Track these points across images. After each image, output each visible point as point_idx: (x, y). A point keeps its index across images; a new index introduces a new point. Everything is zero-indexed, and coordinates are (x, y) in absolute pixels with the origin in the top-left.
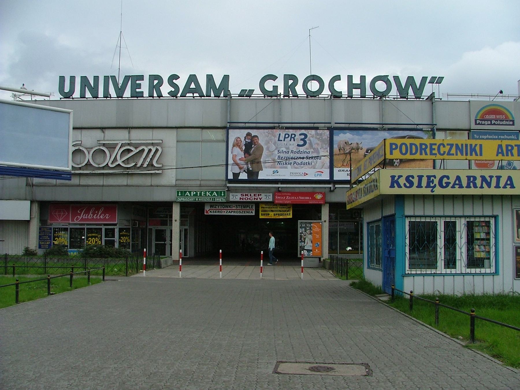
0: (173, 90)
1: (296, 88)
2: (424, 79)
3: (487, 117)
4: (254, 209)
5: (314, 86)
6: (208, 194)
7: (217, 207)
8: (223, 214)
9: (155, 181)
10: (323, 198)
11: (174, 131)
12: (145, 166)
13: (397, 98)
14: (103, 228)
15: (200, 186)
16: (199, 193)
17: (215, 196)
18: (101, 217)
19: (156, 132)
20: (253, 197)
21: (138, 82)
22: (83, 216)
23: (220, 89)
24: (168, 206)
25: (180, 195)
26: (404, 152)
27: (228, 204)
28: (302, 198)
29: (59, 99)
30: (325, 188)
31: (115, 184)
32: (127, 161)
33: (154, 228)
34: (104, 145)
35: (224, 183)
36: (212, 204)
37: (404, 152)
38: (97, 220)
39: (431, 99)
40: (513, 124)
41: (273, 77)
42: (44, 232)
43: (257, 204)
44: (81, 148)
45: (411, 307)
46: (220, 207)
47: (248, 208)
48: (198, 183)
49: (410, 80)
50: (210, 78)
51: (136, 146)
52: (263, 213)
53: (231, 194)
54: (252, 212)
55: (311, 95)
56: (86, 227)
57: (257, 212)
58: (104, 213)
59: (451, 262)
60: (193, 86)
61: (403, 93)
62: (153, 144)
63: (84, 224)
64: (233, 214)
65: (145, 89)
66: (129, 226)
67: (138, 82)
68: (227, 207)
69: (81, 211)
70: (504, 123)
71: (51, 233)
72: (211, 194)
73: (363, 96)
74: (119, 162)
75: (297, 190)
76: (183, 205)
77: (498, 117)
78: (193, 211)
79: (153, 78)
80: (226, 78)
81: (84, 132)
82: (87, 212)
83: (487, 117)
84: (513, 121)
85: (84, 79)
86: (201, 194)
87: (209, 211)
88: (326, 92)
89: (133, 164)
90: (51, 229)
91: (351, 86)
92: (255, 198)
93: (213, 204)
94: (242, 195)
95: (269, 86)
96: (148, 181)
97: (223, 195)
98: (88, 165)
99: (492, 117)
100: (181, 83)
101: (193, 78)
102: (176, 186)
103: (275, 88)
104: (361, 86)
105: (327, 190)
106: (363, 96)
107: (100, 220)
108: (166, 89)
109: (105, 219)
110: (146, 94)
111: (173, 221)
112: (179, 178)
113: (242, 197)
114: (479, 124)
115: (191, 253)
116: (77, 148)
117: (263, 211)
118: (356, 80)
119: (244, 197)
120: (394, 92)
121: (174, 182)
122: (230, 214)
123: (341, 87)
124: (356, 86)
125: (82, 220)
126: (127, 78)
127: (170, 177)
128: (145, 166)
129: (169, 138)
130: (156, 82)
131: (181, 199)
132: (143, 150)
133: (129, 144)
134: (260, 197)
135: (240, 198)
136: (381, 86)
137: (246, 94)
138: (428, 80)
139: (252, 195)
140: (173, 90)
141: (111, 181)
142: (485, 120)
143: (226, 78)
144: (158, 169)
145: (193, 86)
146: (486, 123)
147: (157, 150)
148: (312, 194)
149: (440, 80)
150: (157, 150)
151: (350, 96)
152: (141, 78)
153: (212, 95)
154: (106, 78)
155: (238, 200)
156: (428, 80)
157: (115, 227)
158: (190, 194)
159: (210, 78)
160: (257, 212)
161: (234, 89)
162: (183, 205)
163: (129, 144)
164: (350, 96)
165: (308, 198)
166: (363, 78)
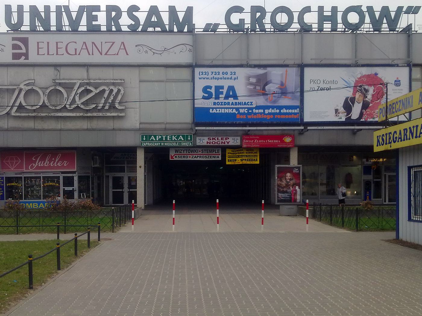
0: (133, 23)
1: (263, 20)
2: (400, 9)
4: (220, 153)
5: (282, 19)
6: (174, 138)
7: (182, 152)
8: (189, 159)
9: (118, 124)
10: (293, 141)
11: (136, 71)
12: (107, 108)
13: (369, 31)
14: (61, 176)
15: (165, 129)
16: (164, 137)
17: (181, 140)
18: (59, 164)
19: (116, 70)
20: (221, 141)
21: (94, 13)
22: (38, 163)
23: (182, 23)
24: (129, 153)
25: (144, 139)
26: (189, 152)
27: (195, 148)
28: (271, 141)
29: (6, 32)
30: (294, 130)
31: (73, 128)
32: (85, 103)
33: (111, 175)
34: (60, 84)
35: (189, 126)
36: (177, 149)
37: (189, 152)
38: (54, 167)
39: (409, 30)
41: (238, 9)
43: (224, 149)
44: (34, 88)
46: (185, 151)
47: (214, 153)
48: (163, 126)
49: (385, 10)
50: (172, 10)
51: (96, 86)
52: (229, 159)
53: (198, 138)
55: (281, 29)
56: (42, 175)
57: (224, 156)
58: (62, 159)
60: (154, 19)
61: (376, 24)
62: (114, 84)
63: (40, 173)
64: (198, 159)
65: (102, 19)
66: (89, 173)
67: (94, 13)
68: (192, 151)
69: (36, 158)
71: (3, 183)
72: (177, 138)
73: (334, 29)
74: (79, 102)
75: (265, 133)
76: (147, 150)
78: (158, 157)
79: (110, 9)
80: (189, 11)
81: (37, 69)
82: (43, 159)
85: (34, 10)
86: (166, 138)
87: (174, 156)
88: (295, 26)
89: (94, 106)
90: (2, 178)
91: (322, 18)
92: (222, 142)
93: (178, 149)
94: (209, 139)
95: (235, 19)
96: (110, 124)
97: (189, 139)
98: (44, 106)
100: (142, 17)
101: (154, 10)
102: (140, 130)
103: (242, 21)
104: (333, 19)
105: (296, 132)
106: (334, 29)
107: (58, 167)
108: (125, 21)
109: (63, 167)
110: (104, 28)
111: (138, 168)
112: (142, 121)
113: (209, 141)
115: (151, 202)
116: (30, 88)
117: (229, 157)
119: (211, 141)
120: (367, 26)
121: (137, 126)
123: (311, 19)
124: (327, 19)
125: (38, 167)
126: (82, 9)
127: (133, 119)
128: (107, 108)
129: (131, 77)
130: (114, 14)
131: (145, 145)
132: (104, 91)
133: (88, 84)
134: (228, 141)
135: (207, 142)
136: (353, 18)
137: (211, 28)
138: (404, 10)
139: (220, 138)
140: (133, 23)
141: (70, 125)
143: (189, 11)
144: (122, 111)
145: (154, 19)
147: (119, 91)
148: (280, 137)
149: (413, 10)
150: (119, 91)
151: (321, 29)
152: (97, 8)
153: (175, 30)
154: (58, 8)
155: (205, 144)
156: (404, 10)
157: (74, 175)
158: (156, 138)
159: (172, 10)
160: (224, 156)
161: (199, 22)
162: (147, 150)
163: (88, 84)
164: (321, 29)
165: (277, 141)
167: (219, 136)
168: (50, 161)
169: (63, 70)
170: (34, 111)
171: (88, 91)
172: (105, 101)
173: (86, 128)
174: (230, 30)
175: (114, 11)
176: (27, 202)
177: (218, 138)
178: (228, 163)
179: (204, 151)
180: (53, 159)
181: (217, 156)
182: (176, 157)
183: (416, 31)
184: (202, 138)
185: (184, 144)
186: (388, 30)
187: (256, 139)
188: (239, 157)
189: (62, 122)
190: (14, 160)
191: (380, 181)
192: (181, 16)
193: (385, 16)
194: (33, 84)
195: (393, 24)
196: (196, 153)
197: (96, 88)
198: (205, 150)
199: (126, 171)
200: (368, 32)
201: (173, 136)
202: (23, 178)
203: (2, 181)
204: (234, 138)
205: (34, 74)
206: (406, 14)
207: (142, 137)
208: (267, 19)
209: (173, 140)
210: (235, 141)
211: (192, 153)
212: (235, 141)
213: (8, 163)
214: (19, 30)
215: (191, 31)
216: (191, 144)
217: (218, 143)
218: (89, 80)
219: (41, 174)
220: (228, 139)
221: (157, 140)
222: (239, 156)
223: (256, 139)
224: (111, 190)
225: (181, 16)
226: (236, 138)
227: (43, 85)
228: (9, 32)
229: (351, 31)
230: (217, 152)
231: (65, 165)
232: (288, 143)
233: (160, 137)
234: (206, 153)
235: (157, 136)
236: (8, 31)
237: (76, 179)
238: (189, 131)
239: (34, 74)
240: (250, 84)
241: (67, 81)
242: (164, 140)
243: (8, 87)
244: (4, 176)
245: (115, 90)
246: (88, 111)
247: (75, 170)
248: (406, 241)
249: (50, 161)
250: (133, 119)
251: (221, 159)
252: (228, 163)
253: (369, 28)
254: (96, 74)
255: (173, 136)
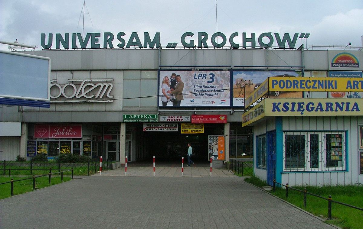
2: (296, 35)
3: (340, 61)
5: (219, 40)
7: (151, 126)
9: (108, 108)
10: (225, 119)
13: (277, 49)
14: (72, 141)
16: (139, 116)
17: (150, 118)
18: (71, 134)
19: (108, 72)
21: (96, 38)
22: (58, 133)
23: (154, 43)
24: (117, 125)
25: (125, 117)
27: (160, 123)
28: (211, 119)
29: (41, 50)
31: (80, 110)
33: (108, 141)
34: (73, 82)
35: (156, 109)
36: (148, 124)
38: (68, 136)
40: (358, 67)
41: (191, 34)
42: (31, 144)
43: (180, 124)
45: (287, 195)
46: (153, 125)
48: (138, 109)
49: (287, 36)
50: (146, 35)
53: (161, 117)
54: (176, 129)
55: (217, 46)
56: (60, 141)
58: (73, 130)
59: (315, 163)
60: (135, 40)
61: (281, 45)
62: (106, 82)
63: (58, 139)
64: (162, 131)
65: (101, 42)
67: (96, 38)
69: (57, 130)
70: (352, 65)
71: (35, 145)
72: (147, 117)
73: (253, 47)
75: (207, 114)
76: (128, 125)
77: (348, 61)
78: (135, 129)
79: (107, 34)
80: (158, 35)
81: (59, 73)
82: (61, 130)
83: (340, 61)
84: (358, 64)
85: (59, 36)
86: (140, 117)
87: (146, 129)
89: (93, 96)
90: (35, 142)
91: (245, 40)
93: (149, 124)
95: (188, 40)
97: (155, 117)
98: (62, 96)
99: (344, 61)
101: (134, 35)
102: (123, 111)
103: (192, 41)
104: (252, 40)
105: (228, 113)
106: (253, 47)
107: (70, 135)
108: (116, 43)
109: (73, 135)
111: (121, 136)
112: (124, 106)
114: (334, 66)
116: (54, 85)
118: (249, 36)
119: (171, 119)
120: (275, 44)
121: (121, 109)
122: (160, 131)
123: (238, 41)
126: (89, 35)
129: (118, 77)
131: (126, 121)
132: (100, 86)
133: (90, 82)
134: (182, 118)
135: (168, 120)
136: (266, 40)
137: (172, 46)
139: (176, 117)
140: (121, 43)
142: (338, 64)
143: (158, 35)
144: (110, 99)
145: (135, 40)
146: (339, 65)
147: (110, 86)
148: (217, 116)
149: (307, 36)
150: (110, 86)
151: (244, 47)
152: (98, 34)
153: (148, 47)
154: (74, 35)
155: (166, 121)
157: (80, 141)
158: (133, 117)
159: (146, 35)
161: (164, 43)
162: (128, 125)
163: (90, 82)
164: (244, 47)
165: (215, 119)
166: (253, 35)
167: (176, 116)
168: (65, 131)
169: (75, 73)
170: (56, 99)
171: (90, 86)
172: (303, 171)
173: (88, 110)
174: (185, 47)
175: (109, 37)
176: (50, 158)
177: (175, 117)
178: (182, 133)
179: (166, 125)
180: (67, 130)
181: (175, 128)
182: (147, 129)
183: (308, 49)
184: (164, 117)
185: (152, 121)
186: (289, 48)
187: (201, 117)
188: (190, 128)
189: (73, 106)
190: (43, 131)
191: (125, 166)
192: (152, 38)
193: (287, 39)
194: (56, 82)
195: (292, 44)
196: (160, 127)
197: (95, 84)
198: (167, 125)
199: (117, 139)
200: (276, 49)
201: (145, 116)
202: (60, 142)
203: (35, 144)
204: (186, 117)
205: (57, 76)
206: (301, 38)
207: (124, 116)
208: (209, 43)
209: (145, 118)
210: (187, 119)
211: (158, 127)
212: (187, 119)
213: (39, 132)
214: (50, 48)
215: (159, 46)
216: (156, 121)
217: (175, 120)
218: (91, 79)
219: (60, 140)
220: (182, 117)
221: (134, 118)
222: (190, 128)
223: (201, 117)
224: (107, 152)
225: (152, 38)
226: (187, 117)
227: (62, 83)
228: (43, 50)
229: (265, 48)
230: (175, 126)
231: (75, 134)
232: (223, 120)
233: (136, 116)
234: (168, 127)
235: (134, 116)
236: (42, 49)
237: (81, 143)
238: (156, 112)
239: (57, 76)
240: (253, 155)
241: (77, 81)
242: (139, 117)
243: (227, 144)
244: (37, 141)
245: (107, 86)
246: (89, 99)
247: (81, 137)
248: (302, 185)
249: (65, 131)
250: (118, 105)
251: (182, 133)
252: (182, 133)
253: (277, 47)
254: (96, 76)
255: (145, 116)
